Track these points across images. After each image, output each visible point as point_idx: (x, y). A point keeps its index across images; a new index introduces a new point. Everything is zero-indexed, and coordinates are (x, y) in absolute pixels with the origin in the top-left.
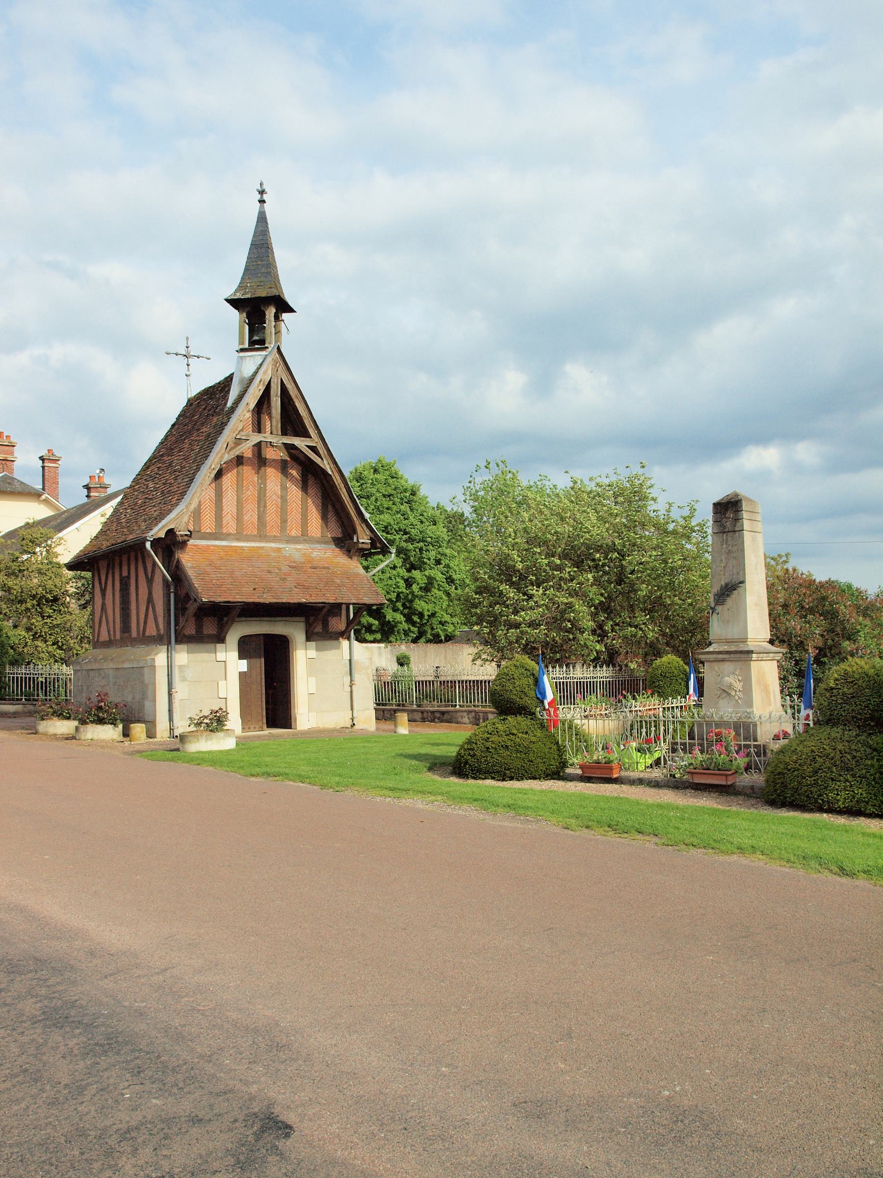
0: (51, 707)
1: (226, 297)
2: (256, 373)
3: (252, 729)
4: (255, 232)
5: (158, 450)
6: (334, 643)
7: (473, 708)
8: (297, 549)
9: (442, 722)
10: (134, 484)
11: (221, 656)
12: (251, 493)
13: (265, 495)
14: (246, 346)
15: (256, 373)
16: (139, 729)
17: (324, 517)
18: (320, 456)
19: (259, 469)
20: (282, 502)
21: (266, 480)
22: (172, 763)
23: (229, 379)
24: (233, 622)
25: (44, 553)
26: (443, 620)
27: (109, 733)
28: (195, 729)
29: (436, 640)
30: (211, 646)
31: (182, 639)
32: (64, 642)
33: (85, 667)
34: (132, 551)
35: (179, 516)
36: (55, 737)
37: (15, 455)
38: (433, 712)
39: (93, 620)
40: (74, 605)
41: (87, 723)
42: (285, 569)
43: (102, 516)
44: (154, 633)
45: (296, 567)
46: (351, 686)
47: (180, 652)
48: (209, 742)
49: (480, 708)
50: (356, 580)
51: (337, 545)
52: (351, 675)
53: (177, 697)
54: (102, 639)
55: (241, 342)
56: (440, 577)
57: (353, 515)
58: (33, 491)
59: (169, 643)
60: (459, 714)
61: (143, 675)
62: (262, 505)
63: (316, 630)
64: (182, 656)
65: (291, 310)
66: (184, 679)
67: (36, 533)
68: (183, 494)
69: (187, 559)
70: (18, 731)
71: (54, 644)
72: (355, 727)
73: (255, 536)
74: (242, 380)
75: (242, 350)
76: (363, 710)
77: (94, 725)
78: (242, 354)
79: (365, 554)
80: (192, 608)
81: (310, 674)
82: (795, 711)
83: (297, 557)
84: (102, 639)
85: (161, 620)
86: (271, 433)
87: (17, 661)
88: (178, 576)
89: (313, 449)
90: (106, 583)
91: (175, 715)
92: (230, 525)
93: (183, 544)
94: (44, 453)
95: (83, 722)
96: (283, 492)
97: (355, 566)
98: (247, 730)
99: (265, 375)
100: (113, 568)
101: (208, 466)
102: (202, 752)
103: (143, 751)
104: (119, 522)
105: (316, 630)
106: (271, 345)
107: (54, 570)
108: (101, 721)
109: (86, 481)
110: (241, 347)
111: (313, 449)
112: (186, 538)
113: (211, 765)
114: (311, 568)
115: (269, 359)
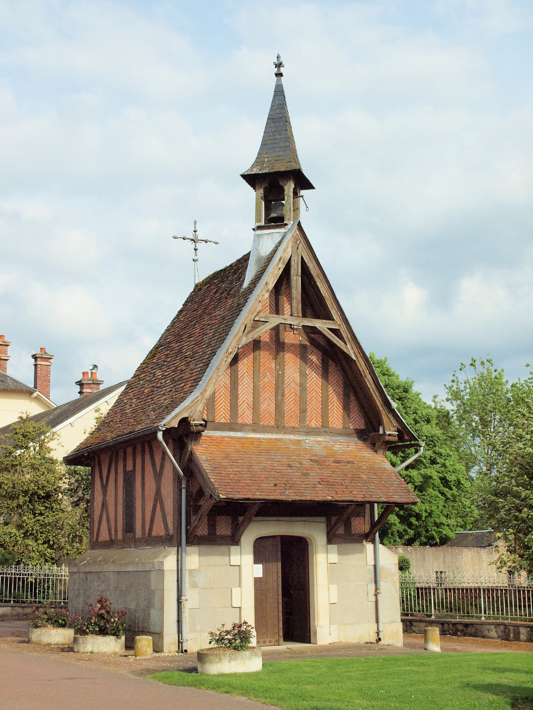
0: (46, 613)
1: (242, 172)
2: (275, 251)
3: (267, 643)
4: (272, 106)
5: (164, 337)
7: (501, 621)
8: (318, 442)
9: (465, 635)
10: (138, 373)
11: (235, 559)
12: (268, 380)
13: (283, 383)
14: (263, 223)
15: (275, 251)
16: (144, 642)
17: (346, 408)
18: (341, 338)
19: (277, 353)
20: (300, 390)
21: (284, 365)
22: (193, 688)
23: (246, 259)
24: (250, 521)
25: (37, 448)
26: (438, 521)
27: (110, 645)
28: (216, 646)
29: (430, 542)
30: (224, 548)
31: (193, 540)
32: (56, 541)
33: (83, 569)
34: (144, 442)
35: (194, 403)
36: (49, 648)
37: (9, 354)
38: (455, 624)
39: (90, 516)
40: (66, 502)
41: (87, 634)
42: (307, 464)
43: (96, 411)
44: (162, 533)
45: (317, 461)
46: (376, 596)
47: (191, 554)
48: (233, 663)
49: (509, 621)
50: (378, 476)
51: (360, 438)
52: (376, 582)
53: (187, 606)
54: (101, 539)
55: (258, 220)
56: (435, 475)
57: (378, 404)
58: (25, 389)
59: (179, 545)
60: (486, 627)
61: (149, 580)
62: (280, 392)
63: (338, 532)
64: (193, 558)
65: (309, 186)
66: (194, 585)
67: (30, 427)
68: (196, 381)
69: (200, 451)
70: (9, 639)
71: (44, 543)
72: (381, 643)
73: (272, 427)
74: (259, 260)
75: (259, 228)
77: (95, 637)
78: (259, 232)
79: (392, 447)
80: (206, 505)
81: (331, 581)
82: (171, 552)
83: (319, 450)
84: (101, 539)
85: (170, 519)
86: (292, 315)
87: (7, 560)
88: (190, 469)
89: (335, 332)
90: (108, 476)
91: (184, 626)
92: (245, 415)
93: (198, 435)
94: (37, 352)
95: (81, 631)
96: (304, 381)
97: (382, 460)
98: (261, 643)
99: (285, 252)
100: (117, 462)
101: (225, 350)
102: (225, 675)
103: (157, 671)
104: (123, 412)
105: (338, 532)
106: (290, 223)
107: (47, 465)
108: (103, 632)
109: (79, 377)
110: (259, 224)
111: (335, 332)
112: (200, 428)
113: (243, 694)
114: (334, 462)
115: (289, 236)
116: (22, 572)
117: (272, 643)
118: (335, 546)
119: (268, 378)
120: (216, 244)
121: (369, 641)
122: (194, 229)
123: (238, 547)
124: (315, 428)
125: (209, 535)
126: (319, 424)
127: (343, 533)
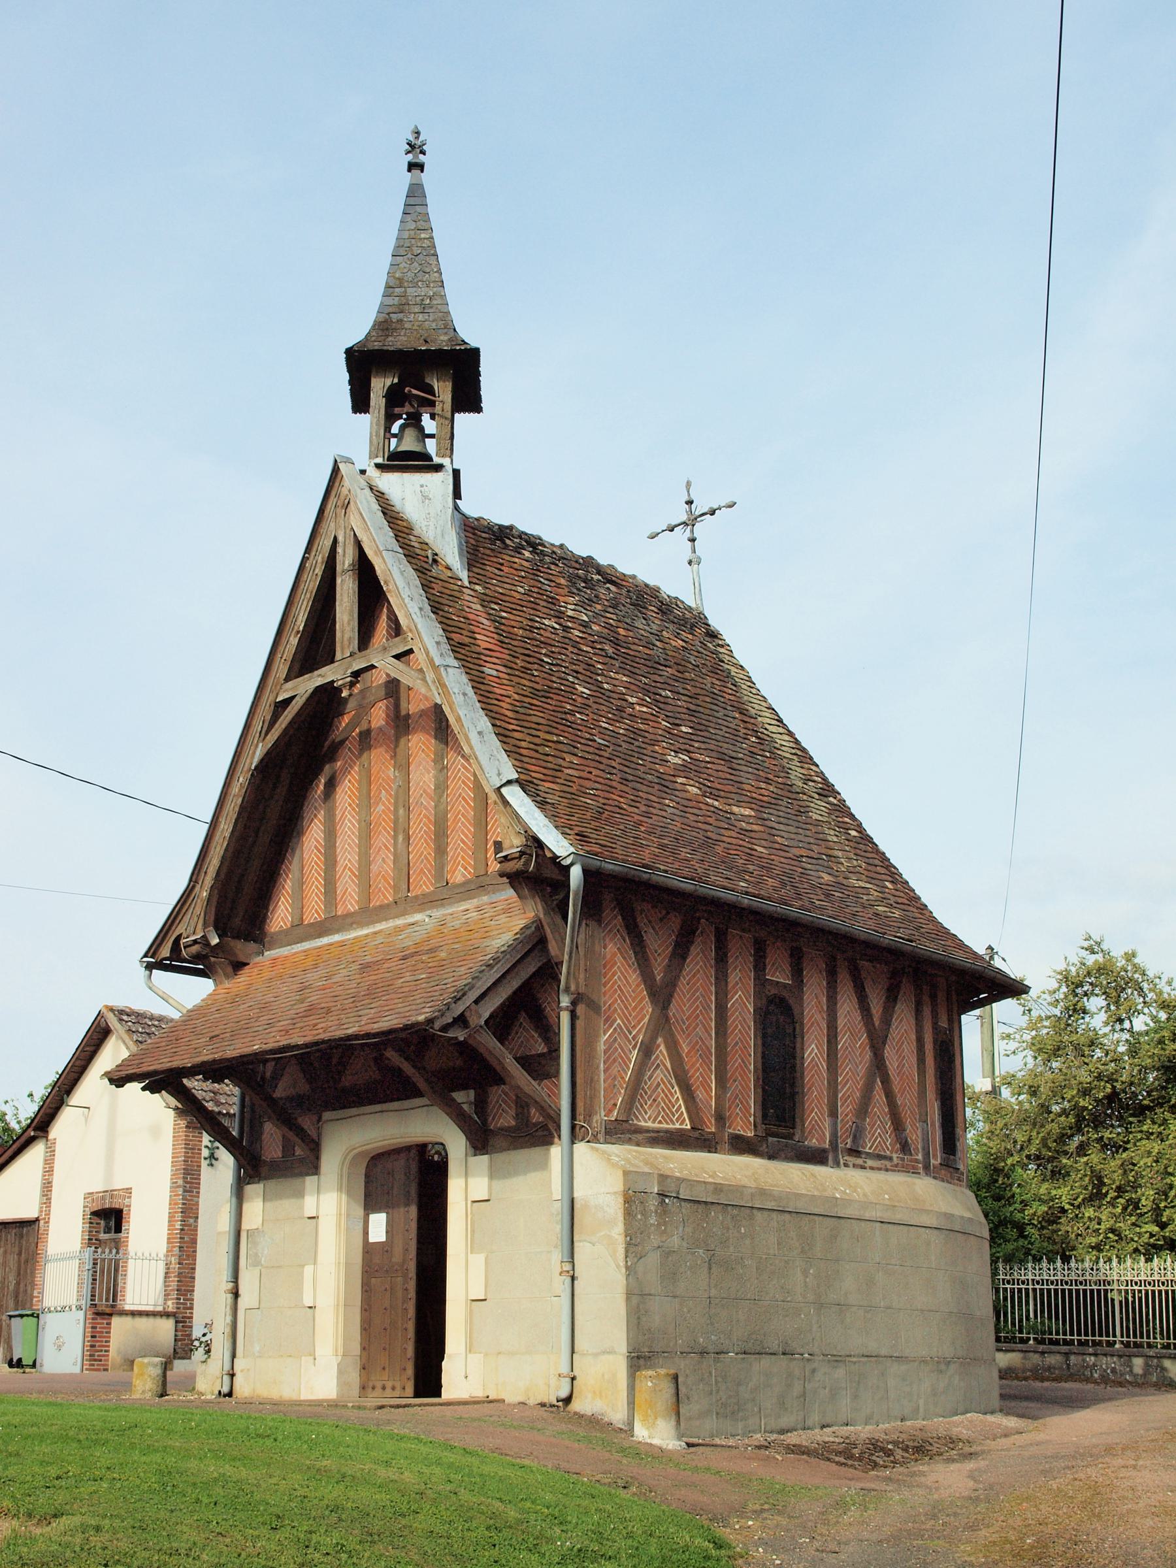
6: (535, 1152)
11: (309, 1204)
12: (383, 807)
30: (296, 1182)
76: (596, 1355)
81: (473, 1246)
92: (349, 898)
116: (1088, 1278)
118: (485, 1158)
119: (384, 804)
120: (730, 506)
121: (545, 1400)
122: (686, 498)
127: (513, 1123)
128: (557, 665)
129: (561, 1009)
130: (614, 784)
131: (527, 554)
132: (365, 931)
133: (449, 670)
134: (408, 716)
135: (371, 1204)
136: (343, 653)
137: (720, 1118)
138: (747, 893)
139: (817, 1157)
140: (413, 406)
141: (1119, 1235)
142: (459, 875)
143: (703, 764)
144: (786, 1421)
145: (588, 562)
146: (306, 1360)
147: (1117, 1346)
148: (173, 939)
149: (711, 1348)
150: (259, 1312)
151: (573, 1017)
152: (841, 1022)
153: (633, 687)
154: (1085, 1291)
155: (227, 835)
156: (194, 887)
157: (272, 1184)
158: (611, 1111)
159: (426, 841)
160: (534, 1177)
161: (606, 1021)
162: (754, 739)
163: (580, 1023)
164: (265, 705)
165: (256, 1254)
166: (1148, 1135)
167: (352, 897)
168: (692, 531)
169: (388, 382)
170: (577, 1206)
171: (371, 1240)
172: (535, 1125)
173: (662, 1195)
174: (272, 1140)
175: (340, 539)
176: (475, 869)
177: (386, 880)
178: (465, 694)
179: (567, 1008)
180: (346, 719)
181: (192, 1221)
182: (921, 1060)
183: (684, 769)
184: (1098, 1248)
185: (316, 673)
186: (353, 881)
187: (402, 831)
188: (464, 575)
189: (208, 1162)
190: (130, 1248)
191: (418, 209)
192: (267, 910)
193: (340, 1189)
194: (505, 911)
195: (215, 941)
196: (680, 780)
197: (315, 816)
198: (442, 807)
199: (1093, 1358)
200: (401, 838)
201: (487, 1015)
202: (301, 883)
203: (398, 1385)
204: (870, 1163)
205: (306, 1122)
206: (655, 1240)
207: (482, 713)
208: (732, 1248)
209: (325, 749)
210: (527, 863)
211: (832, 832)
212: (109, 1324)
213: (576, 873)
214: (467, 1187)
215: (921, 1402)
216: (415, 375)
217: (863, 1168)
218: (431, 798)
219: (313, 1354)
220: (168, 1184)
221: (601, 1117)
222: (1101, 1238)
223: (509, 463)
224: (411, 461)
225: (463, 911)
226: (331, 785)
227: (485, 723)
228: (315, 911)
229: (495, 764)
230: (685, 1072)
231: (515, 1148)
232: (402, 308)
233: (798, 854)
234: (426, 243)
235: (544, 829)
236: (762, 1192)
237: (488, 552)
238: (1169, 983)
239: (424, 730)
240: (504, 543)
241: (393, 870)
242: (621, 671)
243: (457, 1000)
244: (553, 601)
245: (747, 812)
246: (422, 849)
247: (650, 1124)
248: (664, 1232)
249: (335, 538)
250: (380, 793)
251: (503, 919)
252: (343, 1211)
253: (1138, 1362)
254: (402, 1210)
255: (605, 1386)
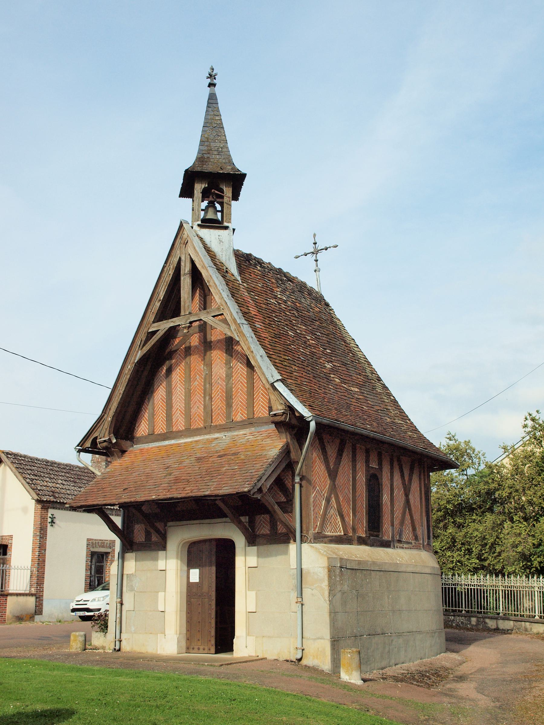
6: (281, 547)
11: (161, 564)
12: (198, 383)
19: (205, 352)
30: (153, 553)
66: (132, 589)
76: (315, 639)
81: (250, 586)
92: (180, 423)
117: (206, 651)
118: (255, 548)
119: (198, 382)
120: (335, 247)
121: (288, 659)
122: (313, 242)
123: (165, 552)
124: (241, 422)
125: (145, 541)
126: (245, 417)
128: (280, 322)
129: (296, 483)
130: (311, 379)
131: (259, 268)
132: (189, 440)
133: (244, 325)
134: (211, 342)
135: (191, 563)
136: (185, 312)
137: (354, 530)
138: (371, 431)
139: (386, 544)
140: (213, 198)
141: (462, 564)
142: (239, 417)
143: (337, 368)
144: (383, 664)
145: (280, 271)
146: (160, 636)
147: (463, 612)
148: (92, 438)
149: (358, 634)
150: (134, 612)
151: (301, 486)
152: (395, 484)
153: (308, 332)
154: (449, 588)
155: (122, 392)
156: (104, 415)
157: (139, 553)
158: (315, 528)
159: (221, 400)
160: (280, 558)
161: (313, 488)
162: (351, 355)
163: (304, 489)
164: (143, 334)
165: (132, 586)
166: (474, 521)
167: (181, 423)
168: (316, 257)
169: (203, 186)
170: (303, 572)
171: (191, 581)
172: (280, 534)
173: (341, 567)
174: (139, 532)
175: (183, 258)
176: (247, 415)
177: (199, 417)
178: (252, 337)
179: (298, 483)
180: (177, 341)
181: (43, 551)
182: (421, 499)
183: (334, 370)
184: (452, 569)
185: (170, 320)
186: (181, 416)
187: (208, 394)
188: (239, 278)
189: (50, 524)
190: (12, 564)
191: (214, 105)
192: (135, 426)
193: (177, 558)
194: (268, 437)
195: (114, 441)
196: (332, 376)
197: (161, 384)
198: (229, 385)
199: (453, 617)
200: (207, 398)
201: (268, 487)
202: (153, 415)
203: (206, 648)
204: (405, 546)
205: (159, 525)
206: (339, 588)
207: (260, 346)
208: (364, 589)
209: (166, 353)
210: (286, 417)
211: (386, 398)
212: (6, 600)
213: (313, 425)
214: (245, 561)
215: (427, 650)
216: (213, 183)
217: (403, 548)
218: (224, 381)
219: (164, 633)
220: (32, 534)
221: (312, 532)
222: (454, 564)
223: (258, 227)
224: (208, 223)
225: (244, 435)
226: (169, 371)
227: (262, 352)
228: (161, 427)
229: (269, 372)
230: (341, 509)
231: (271, 544)
232: (209, 151)
233: (377, 409)
234: (219, 122)
235: (296, 403)
236: (374, 563)
237: (245, 267)
238: (483, 455)
239: (220, 349)
240: (249, 262)
241: (204, 412)
242: (302, 324)
243: (259, 481)
244: (272, 291)
245: (357, 390)
246: (218, 404)
247: (329, 534)
248: (342, 584)
249: (180, 258)
250: (196, 376)
251: (269, 441)
252: (179, 568)
253: (474, 620)
254: (207, 568)
255: (319, 655)
